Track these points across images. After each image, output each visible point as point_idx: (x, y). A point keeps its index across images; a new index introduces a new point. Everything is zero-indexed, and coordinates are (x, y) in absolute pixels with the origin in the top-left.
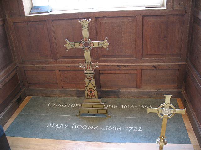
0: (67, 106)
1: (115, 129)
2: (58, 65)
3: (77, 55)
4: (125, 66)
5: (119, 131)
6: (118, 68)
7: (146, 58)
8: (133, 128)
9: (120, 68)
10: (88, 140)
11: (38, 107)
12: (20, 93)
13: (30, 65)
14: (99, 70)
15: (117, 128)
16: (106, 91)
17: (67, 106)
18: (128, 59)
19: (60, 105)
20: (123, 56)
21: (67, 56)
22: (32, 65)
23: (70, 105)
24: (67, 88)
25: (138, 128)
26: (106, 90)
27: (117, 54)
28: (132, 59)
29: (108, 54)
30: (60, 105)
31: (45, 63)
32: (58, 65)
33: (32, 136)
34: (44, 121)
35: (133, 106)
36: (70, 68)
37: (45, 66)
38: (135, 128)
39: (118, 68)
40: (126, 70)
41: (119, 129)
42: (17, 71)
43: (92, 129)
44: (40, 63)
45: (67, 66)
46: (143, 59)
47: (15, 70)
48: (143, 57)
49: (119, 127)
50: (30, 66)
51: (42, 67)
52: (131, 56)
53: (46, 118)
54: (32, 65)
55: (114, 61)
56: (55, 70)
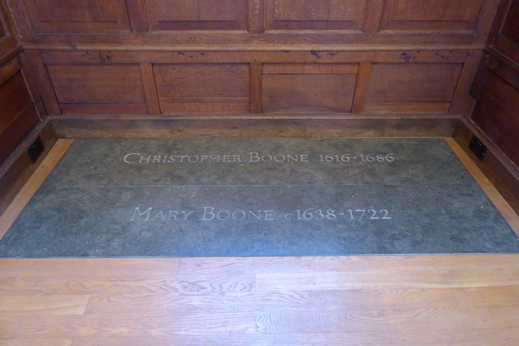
0: (178, 159)
1: (320, 217)
2: (147, 48)
3: (204, 17)
4: (332, 53)
5: (333, 224)
6: (312, 58)
7: (389, 32)
8: (367, 211)
9: (319, 57)
10: (257, 251)
11: (96, 168)
12: (38, 130)
13: (61, 47)
14: (263, 64)
15: (325, 213)
16: (276, 120)
17: (178, 159)
18: (343, 32)
19: (157, 159)
20: (329, 24)
21: (128, 63)
22: (68, 48)
23: (186, 160)
24: (172, 113)
25: (377, 210)
26: (275, 118)
27: (315, 18)
28: (352, 32)
29: (292, 18)
30: (157, 159)
31: (105, 41)
32: (147, 48)
33: (88, 252)
34: (118, 204)
35: (347, 156)
36: (181, 58)
37: (109, 51)
38: (372, 212)
39: (312, 58)
40: (332, 63)
41: (330, 216)
42: (20, 63)
43: (259, 218)
44: (94, 40)
45: (173, 51)
46: (381, 32)
47: (15, 61)
48: (380, 28)
49: (331, 212)
50: (63, 51)
51: (100, 52)
52: (350, 24)
53: (487, 186)
54: (68, 48)
55: (305, 39)
56: (138, 64)
